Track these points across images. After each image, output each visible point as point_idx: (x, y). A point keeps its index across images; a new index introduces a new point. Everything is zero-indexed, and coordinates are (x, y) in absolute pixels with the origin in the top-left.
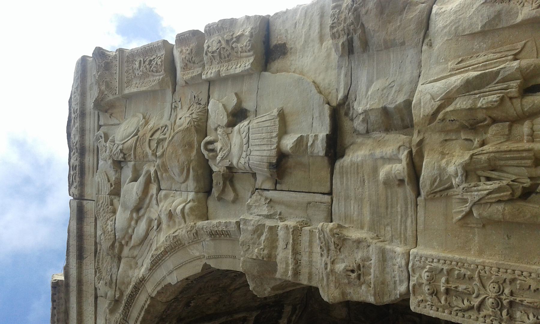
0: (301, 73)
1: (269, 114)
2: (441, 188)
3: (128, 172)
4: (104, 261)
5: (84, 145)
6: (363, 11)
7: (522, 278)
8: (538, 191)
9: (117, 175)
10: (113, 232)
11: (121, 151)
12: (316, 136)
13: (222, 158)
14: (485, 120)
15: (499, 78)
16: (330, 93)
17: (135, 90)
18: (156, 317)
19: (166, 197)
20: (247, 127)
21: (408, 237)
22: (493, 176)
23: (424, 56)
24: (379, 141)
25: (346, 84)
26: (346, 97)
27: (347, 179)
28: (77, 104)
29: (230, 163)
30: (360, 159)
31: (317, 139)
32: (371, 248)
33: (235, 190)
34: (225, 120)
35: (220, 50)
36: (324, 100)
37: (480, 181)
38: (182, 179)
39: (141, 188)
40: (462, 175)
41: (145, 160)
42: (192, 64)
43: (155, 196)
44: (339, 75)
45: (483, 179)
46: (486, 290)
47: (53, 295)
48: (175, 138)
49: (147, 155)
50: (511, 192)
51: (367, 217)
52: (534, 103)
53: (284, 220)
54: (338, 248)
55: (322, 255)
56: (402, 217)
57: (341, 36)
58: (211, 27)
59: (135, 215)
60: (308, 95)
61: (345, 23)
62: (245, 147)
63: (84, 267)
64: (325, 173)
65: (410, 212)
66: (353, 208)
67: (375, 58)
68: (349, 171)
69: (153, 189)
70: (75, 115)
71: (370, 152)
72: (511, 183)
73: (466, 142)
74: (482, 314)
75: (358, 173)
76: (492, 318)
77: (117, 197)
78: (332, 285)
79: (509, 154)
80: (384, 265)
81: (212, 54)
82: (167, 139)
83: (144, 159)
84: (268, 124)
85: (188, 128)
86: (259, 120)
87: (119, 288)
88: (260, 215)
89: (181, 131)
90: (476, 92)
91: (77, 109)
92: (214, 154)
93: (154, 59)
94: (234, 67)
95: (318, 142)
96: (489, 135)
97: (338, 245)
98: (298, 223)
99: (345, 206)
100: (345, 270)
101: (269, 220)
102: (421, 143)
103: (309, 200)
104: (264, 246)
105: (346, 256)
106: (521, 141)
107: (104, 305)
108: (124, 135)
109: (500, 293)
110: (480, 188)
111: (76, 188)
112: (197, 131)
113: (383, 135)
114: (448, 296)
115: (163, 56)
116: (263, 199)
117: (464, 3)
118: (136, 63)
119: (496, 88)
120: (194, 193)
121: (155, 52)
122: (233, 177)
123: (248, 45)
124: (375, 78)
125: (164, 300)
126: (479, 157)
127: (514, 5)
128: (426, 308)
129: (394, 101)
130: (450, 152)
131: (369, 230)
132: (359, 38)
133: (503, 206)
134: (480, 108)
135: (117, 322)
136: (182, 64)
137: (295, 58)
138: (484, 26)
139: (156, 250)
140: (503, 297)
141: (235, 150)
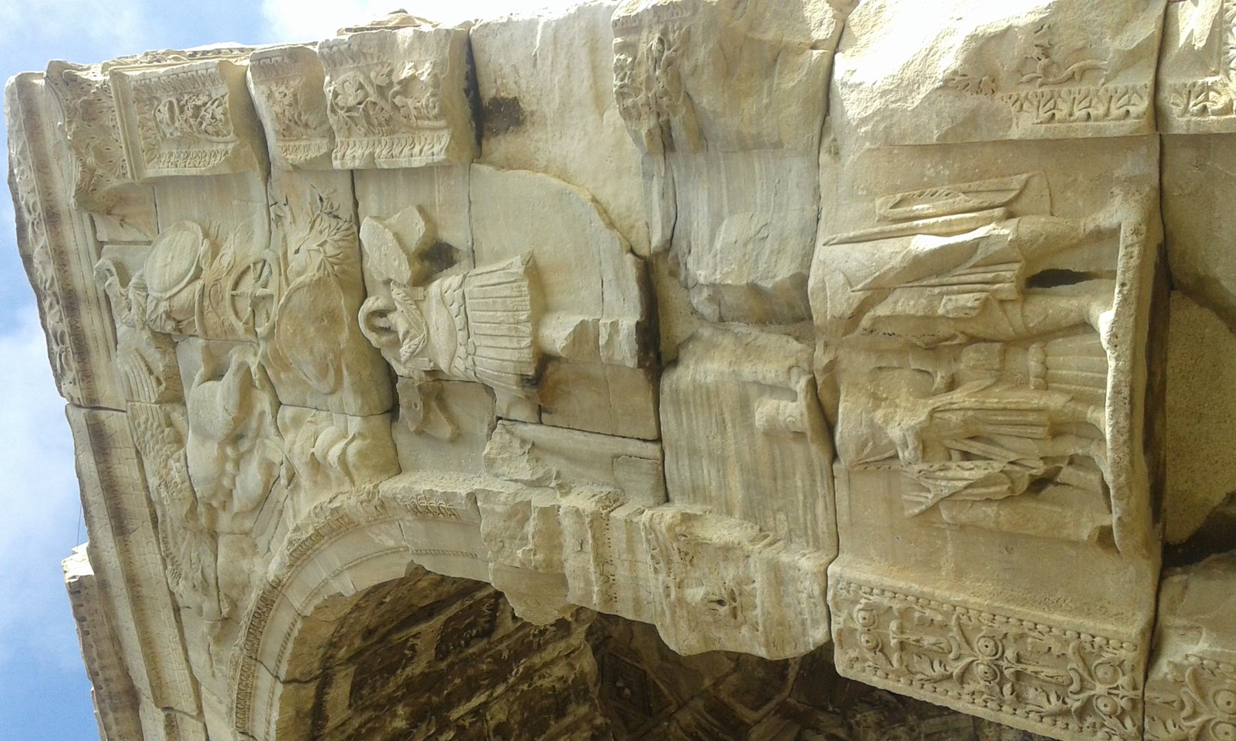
0: (563, 175)
1: (504, 269)
2: (877, 458)
3: (192, 354)
4: (179, 539)
5: (71, 288)
6: (686, 67)
7: (1036, 634)
8: (1058, 480)
9: (167, 358)
10: (187, 484)
11: (169, 315)
12: (614, 325)
13: (412, 353)
14: (953, 337)
15: (978, 257)
16: (632, 227)
17: (172, 172)
18: (319, 647)
19: (297, 422)
20: (459, 292)
21: (821, 535)
22: (974, 451)
23: (824, 178)
24: (747, 345)
25: (665, 216)
26: (669, 244)
27: (689, 416)
28: (33, 190)
29: (432, 364)
30: (710, 379)
31: (617, 332)
32: (751, 560)
33: (451, 419)
34: (404, 271)
35: (366, 106)
36: (621, 243)
37: (950, 458)
38: (325, 387)
39: (234, 399)
40: (915, 449)
41: (230, 337)
42: (301, 129)
43: (269, 418)
44: (648, 192)
45: (955, 455)
46: (972, 649)
47: (76, 607)
48: (295, 300)
49: (232, 330)
50: (1010, 485)
51: (737, 493)
52: (1047, 316)
53: (567, 489)
54: (688, 558)
55: (656, 571)
56: (805, 498)
57: (644, 116)
58: (335, 49)
59: (229, 451)
60: (585, 229)
61: (649, 89)
62: (461, 335)
63: (134, 550)
64: (642, 400)
65: (821, 489)
66: (708, 474)
67: (723, 167)
68: (692, 400)
69: (263, 402)
70: (33, 216)
71: (731, 369)
72: (1009, 468)
73: (919, 377)
74: (969, 688)
75: (710, 406)
76: (985, 696)
77: (177, 406)
78: (683, 625)
79: (1004, 416)
80: (779, 591)
81: (348, 114)
82: (276, 298)
83: (228, 337)
84: (505, 291)
85: (320, 279)
86: (484, 280)
87: (226, 595)
88: (516, 481)
89: (303, 287)
90: (933, 281)
91: (34, 204)
92: (391, 337)
93: (205, 104)
94: (406, 150)
95: (620, 338)
96: (962, 366)
97: (687, 554)
98: (600, 505)
99: (691, 467)
100: (706, 601)
101: (537, 492)
102: (831, 367)
103: (615, 451)
104: (535, 545)
105: (704, 574)
106: (1022, 384)
107: (199, 629)
108: (167, 277)
109: (997, 656)
110: (950, 474)
111: (75, 384)
112: (343, 285)
113: (755, 331)
114: (904, 653)
115: (226, 98)
116: (516, 443)
117: (899, 76)
118: (161, 107)
119: (972, 278)
120: (359, 418)
121: (204, 84)
122: (442, 390)
123: (431, 105)
124: (726, 209)
125: (333, 618)
126: (947, 415)
127: (1003, 103)
128: (864, 671)
129: (770, 274)
130: (891, 397)
131: (745, 519)
132: (684, 124)
133: (995, 508)
134: (942, 317)
135: (237, 663)
136: (277, 125)
137: (544, 137)
138: (943, 137)
139: (297, 529)
140: (1004, 664)
141: (440, 339)
